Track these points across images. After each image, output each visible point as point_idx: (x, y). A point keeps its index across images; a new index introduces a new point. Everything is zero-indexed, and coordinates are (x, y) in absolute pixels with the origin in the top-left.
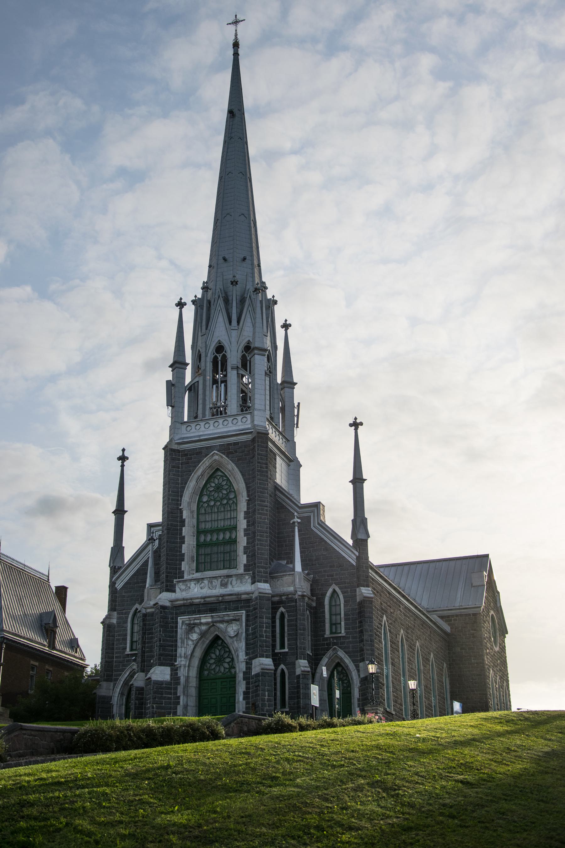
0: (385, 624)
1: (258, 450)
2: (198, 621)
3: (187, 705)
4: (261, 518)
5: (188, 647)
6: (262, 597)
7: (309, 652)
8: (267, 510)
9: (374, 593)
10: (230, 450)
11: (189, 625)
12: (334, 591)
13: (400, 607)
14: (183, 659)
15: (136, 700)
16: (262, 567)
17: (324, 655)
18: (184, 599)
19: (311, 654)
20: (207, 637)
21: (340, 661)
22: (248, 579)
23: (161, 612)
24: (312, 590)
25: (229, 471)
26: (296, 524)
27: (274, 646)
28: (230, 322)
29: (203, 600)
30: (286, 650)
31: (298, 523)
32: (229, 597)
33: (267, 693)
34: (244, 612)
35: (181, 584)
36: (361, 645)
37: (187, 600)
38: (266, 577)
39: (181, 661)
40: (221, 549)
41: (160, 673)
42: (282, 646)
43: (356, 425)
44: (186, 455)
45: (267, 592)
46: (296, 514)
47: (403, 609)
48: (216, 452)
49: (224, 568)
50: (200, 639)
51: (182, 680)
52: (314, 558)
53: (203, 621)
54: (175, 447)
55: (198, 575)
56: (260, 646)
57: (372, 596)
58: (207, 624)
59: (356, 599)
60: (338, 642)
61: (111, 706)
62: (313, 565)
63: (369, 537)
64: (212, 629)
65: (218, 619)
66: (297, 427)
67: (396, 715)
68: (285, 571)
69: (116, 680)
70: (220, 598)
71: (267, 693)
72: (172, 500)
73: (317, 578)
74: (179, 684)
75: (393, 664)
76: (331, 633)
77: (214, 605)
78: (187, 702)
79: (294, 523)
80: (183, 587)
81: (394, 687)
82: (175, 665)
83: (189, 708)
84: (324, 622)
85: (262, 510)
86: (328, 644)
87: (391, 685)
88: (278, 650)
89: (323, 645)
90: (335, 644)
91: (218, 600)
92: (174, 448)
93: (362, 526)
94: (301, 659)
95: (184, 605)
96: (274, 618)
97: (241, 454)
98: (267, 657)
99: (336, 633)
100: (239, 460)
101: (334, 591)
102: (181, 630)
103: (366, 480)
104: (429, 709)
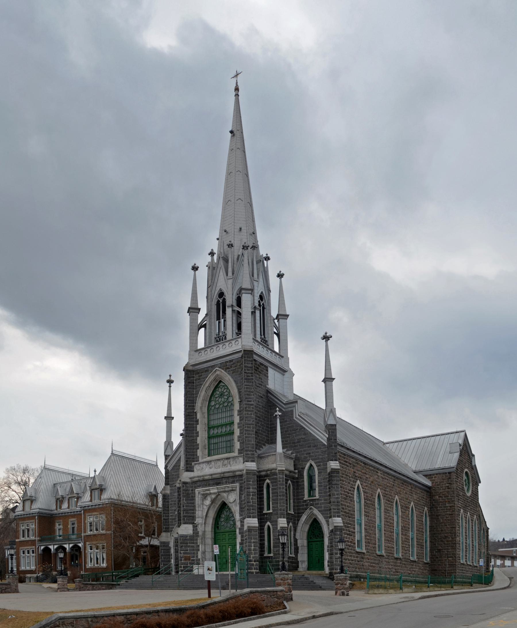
0: (358, 487)
2: (208, 492)
3: (205, 551)
4: (248, 414)
5: (204, 509)
6: (249, 472)
11: (203, 495)
12: (311, 465)
13: (377, 472)
14: (200, 519)
16: (251, 451)
18: (198, 477)
19: (293, 513)
22: (241, 459)
23: (183, 486)
24: (295, 465)
26: (278, 416)
27: (261, 509)
28: (227, 275)
29: (210, 477)
30: (271, 511)
33: (253, 545)
37: (200, 477)
38: (253, 458)
39: (199, 521)
40: (224, 439)
41: (186, 529)
42: (269, 509)
43: (326, 338)
45: (253, 468)
47: (381, 474)
48: (218, 369)
49: (226, 453)
52: (296, 441)
54: (191, 368)
55: (209, 459)
56: (248, 509)
57: (339, 467)
58: (214, 493)
60: (313, 503)
64: (219, 497)
65: (222, 490)
69: (171, 531)
70: (222, 475)
71: (253, 545)
73: (299, 456)
74: (198, 536)
76: (310, 495)
78: (205, 549)
79: (276, 416)
83: (206, 553)
84: (303, 488)
85: (249, 408)
86: (307, 505)
88: (265, 511)
89: (303, 505)
90: (312, 505)
93: (331, 414)
95: (199, 481)
98: (253, 518)
99: (313, 496)
100: (233, 373)
101: (311, 465)
102: (198, 499)
103: (334, 379)
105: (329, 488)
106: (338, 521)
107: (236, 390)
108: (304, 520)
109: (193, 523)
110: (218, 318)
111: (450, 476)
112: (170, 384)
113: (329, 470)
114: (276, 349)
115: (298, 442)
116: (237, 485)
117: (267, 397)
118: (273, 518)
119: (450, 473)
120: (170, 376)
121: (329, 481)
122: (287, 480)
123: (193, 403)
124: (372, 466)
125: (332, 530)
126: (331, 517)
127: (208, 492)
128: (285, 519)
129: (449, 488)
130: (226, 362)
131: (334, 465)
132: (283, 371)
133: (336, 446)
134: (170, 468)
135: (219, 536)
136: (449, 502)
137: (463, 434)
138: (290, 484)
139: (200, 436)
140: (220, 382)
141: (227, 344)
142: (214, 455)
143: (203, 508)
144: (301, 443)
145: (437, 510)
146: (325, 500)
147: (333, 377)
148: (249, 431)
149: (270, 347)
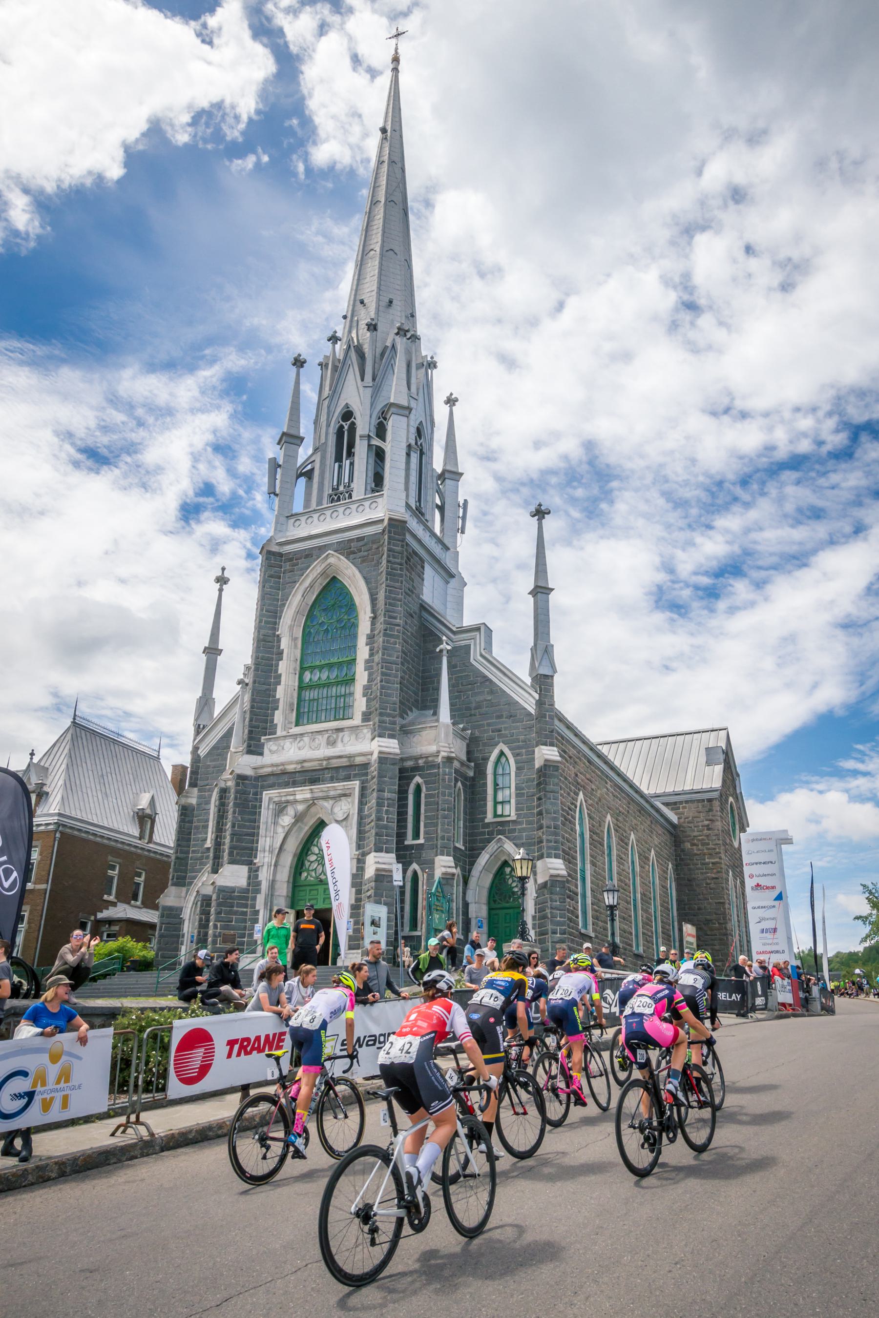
1: (389, 543)
4: (388, 642)
7: (460, 845)
8: (398, 631)
9: (561, 756)
10: (355, 548)
12: (502, 753)
14: (267, 854)
15: (201, 914)
16: (389, 715)
17: (483, 849)
18: (272, 765)
19: (463, 848)
20: (305, 820)
21: (507, 859)
22: (367, 733)
24: (469, 753)
25: (349, 578)
26: (445, 652)
27: (401, 836)
30: (421, 841)
31: (448, 651)
32: (338, 760)
34: (358, 782)
35: (271, 743)
36: (540, 834)
37: (277, 765)
39: (263, 859)
41: (233, 876)
42: (416, 836)
44: (291, 560)
45: (392, 750)
46: (444, 638)
49: (335, 720)
50: (294, 824)
51: (264, 886)
52: (474, 705)
53: (299, 797)
54: (275, 549)
57: (559, 759)
58: (305, 801)
59: (534, 765)
60: (503, 827)
61: (181, 922)
62: (471, 715)
63: (555, 671)
64: (313, 810)
65: (321, 794)
66: (463, 532)
67: (596, 937)
68: (424, 723)
69: (190, 884)
70: (325, 763)
72: (266, 622)
73: (477, 733)
75: (593, 864)
76: (496, 815)
77: (317, 773)
80: (274, 748)
81: (593, 896)
82: (255, 864)
84: (485, 799)
86: (491, 833)
87: (589, 893)
88: (409, 841)
89: (483, 833)
91: (321, 765)
92: (273, 550)
94: (443, 855)
95: (273, 774)
96: (402, 794)
97: (366, 553)
98: (387, 852)
99: (502, 816)
101: (502, 753)
102: (266, 814)
103: (553, 589)
104: (648, 924)
105: (540, 799)
106: (556, 866)
107: (367, 595)
108: (483, 863)
109: (250, 863)
110: (338, 459)
111: (711, 805)
112: (221, 586)
113: (538, 764)
114: (437, 530)
115: (476, 708)
116: (356, 784)
117: (421, 617)
118: (426, 855)
119: (710, 800)
120: (223, 569)
121: (539, 784)
122: (456, 780)
123: (276, 617)
124: (598, 769)
125: (546, 883)
126: (541, 857)
127: (291, 798)
128: (451, 858)
129: (709, 829)
130: (350, 541)
131: (548, 753)
132: (448, 574)
133: (551, 718)
134: (202, 752)
135: (302, 894)
136: (710, 854)
137: (723, 734)
138: (460, 789)
139: (283, 683)
140: (334, 578)
141: (354, 507)
142: (308, 723)
143: (275, 832)
144: (484, 710)
145: (690, 870)
146: (528, 823)
147: (550, 586)
148: (389, 676)
149: (429, 524)
